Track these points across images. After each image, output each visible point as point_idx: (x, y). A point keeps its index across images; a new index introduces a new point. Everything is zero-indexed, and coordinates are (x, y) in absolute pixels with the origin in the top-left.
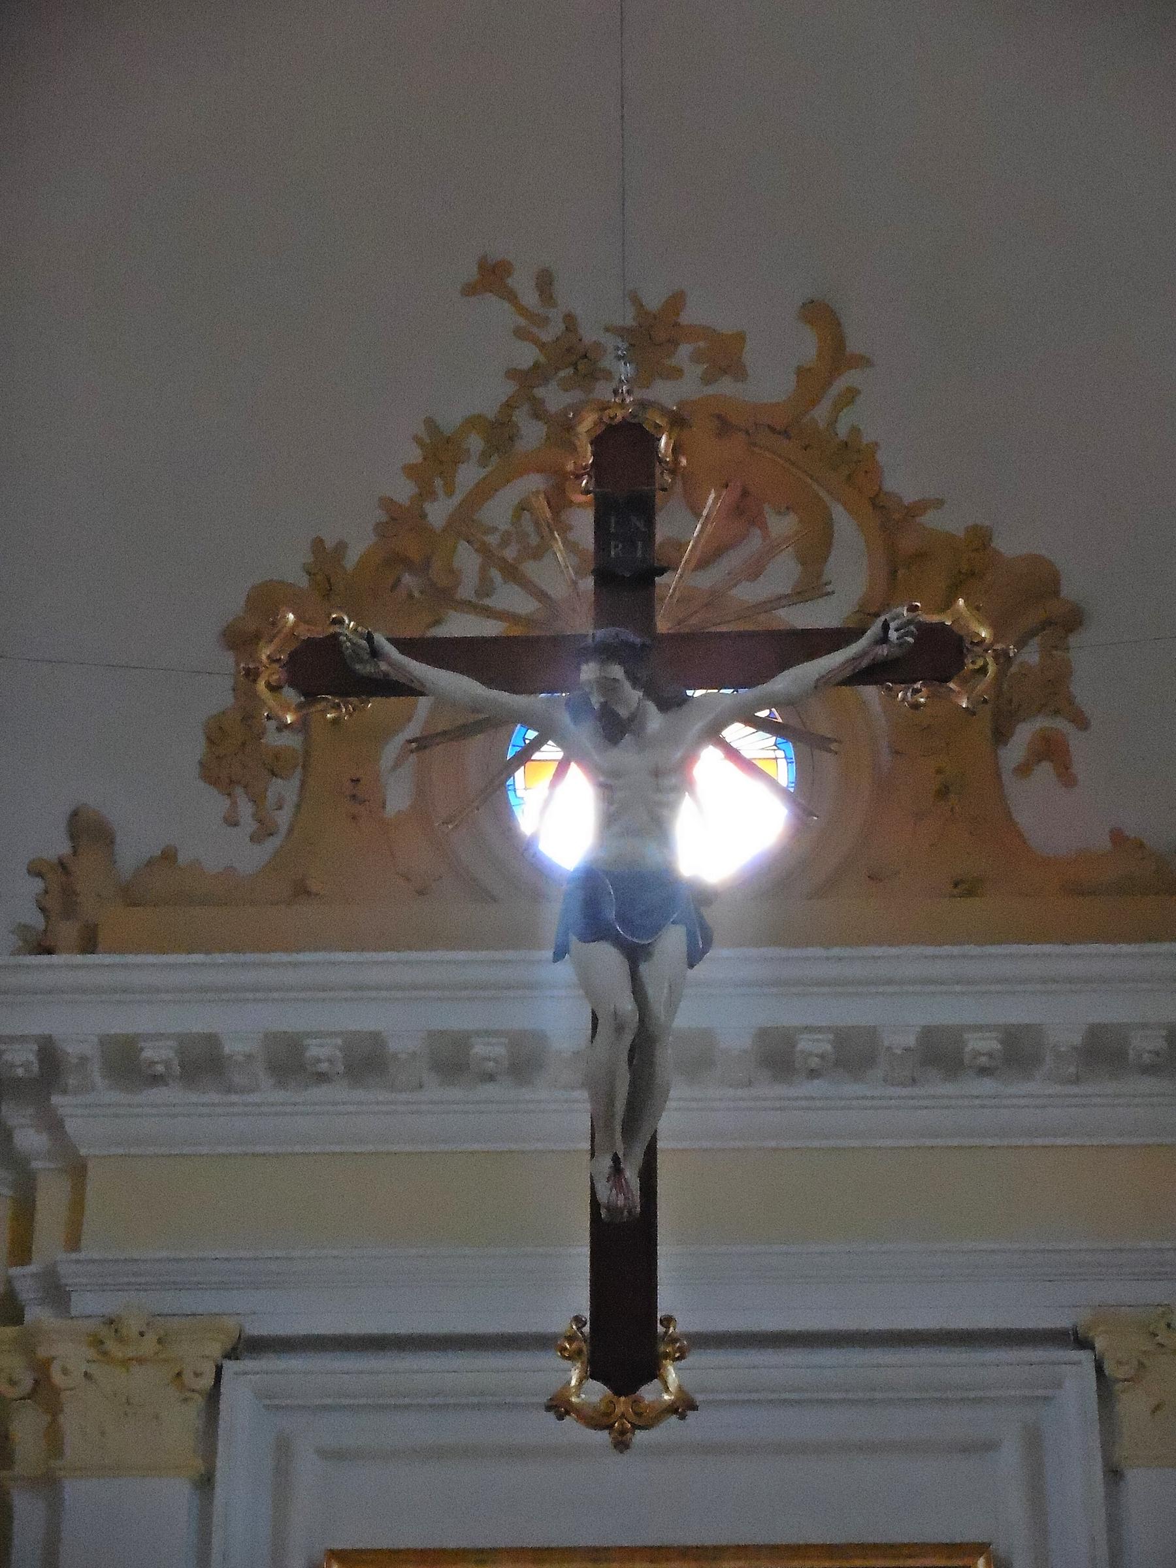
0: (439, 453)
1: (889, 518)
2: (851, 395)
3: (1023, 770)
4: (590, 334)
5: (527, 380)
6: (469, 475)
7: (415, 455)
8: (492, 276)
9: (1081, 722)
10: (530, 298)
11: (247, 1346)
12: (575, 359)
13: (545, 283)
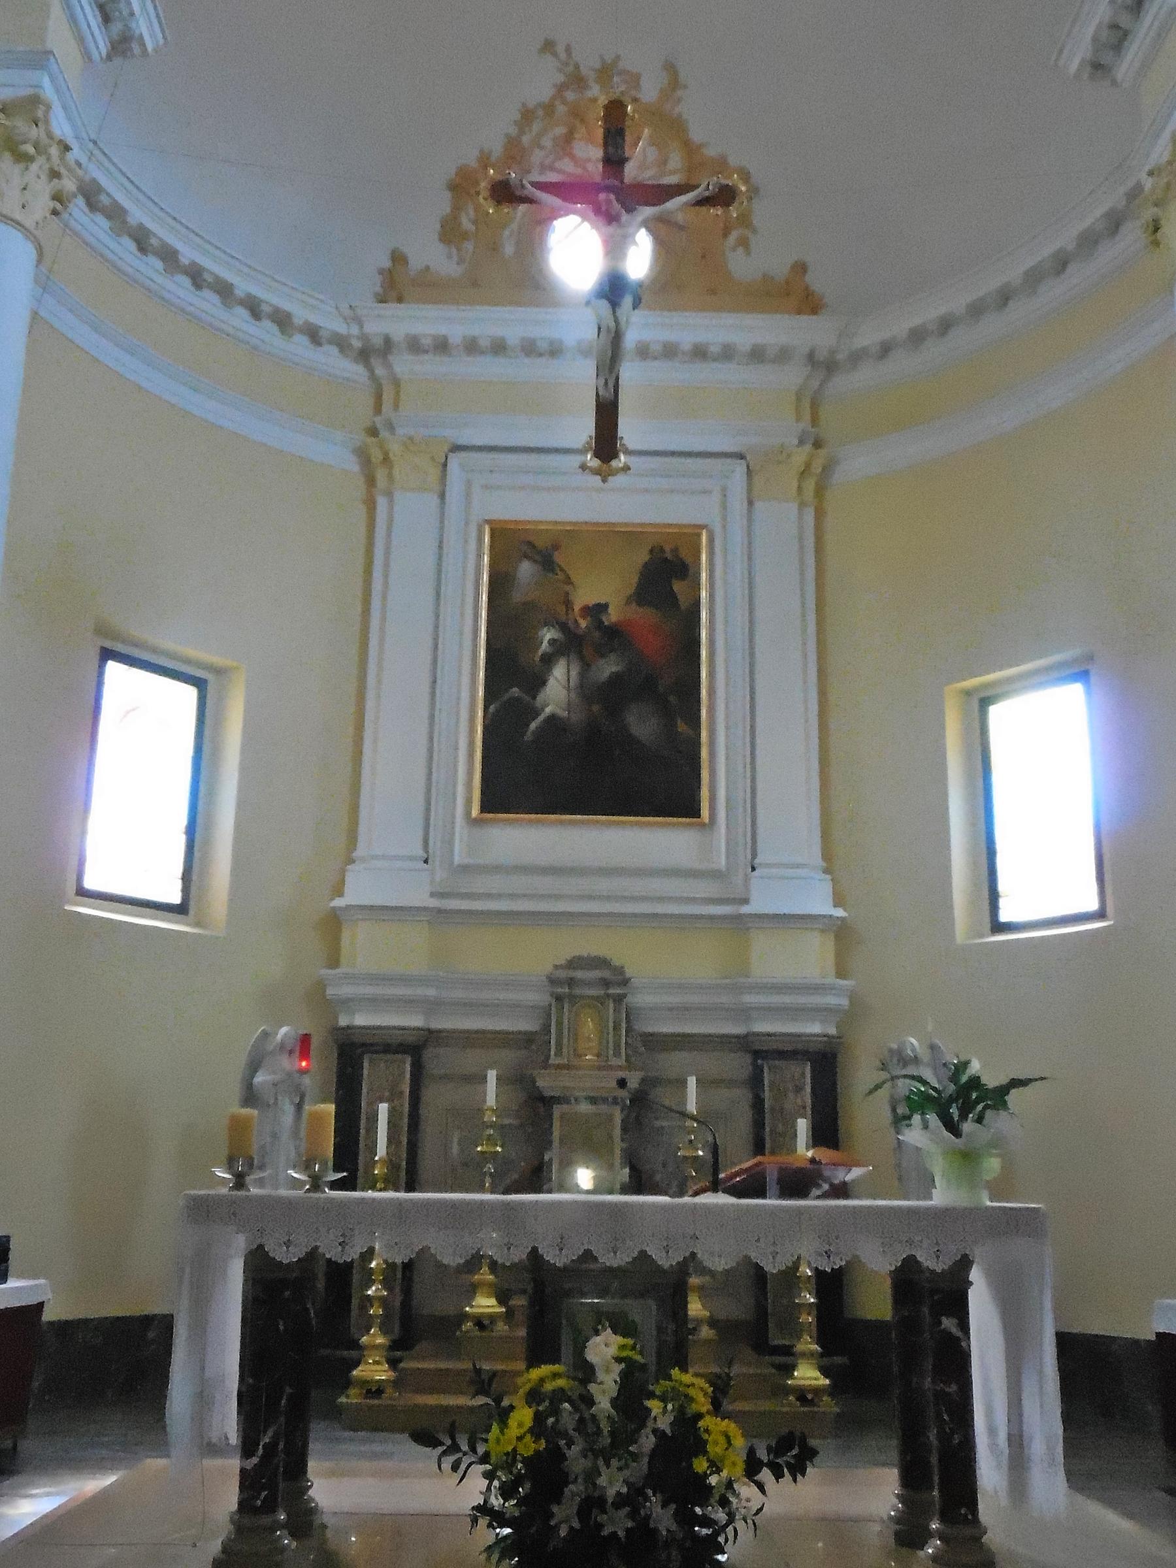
0: (527, 116)
1: (690, 149)
2: (679, 100)
3: (734, 249)
4: (584, 71)
5: (561, 88)
6: (536, 127)
7: (518, 116)
8: (548, 46)
9: (755, 231)
10: (563, 56)
11: (457, 448)
12: (577, 80)
13: (568, 49)
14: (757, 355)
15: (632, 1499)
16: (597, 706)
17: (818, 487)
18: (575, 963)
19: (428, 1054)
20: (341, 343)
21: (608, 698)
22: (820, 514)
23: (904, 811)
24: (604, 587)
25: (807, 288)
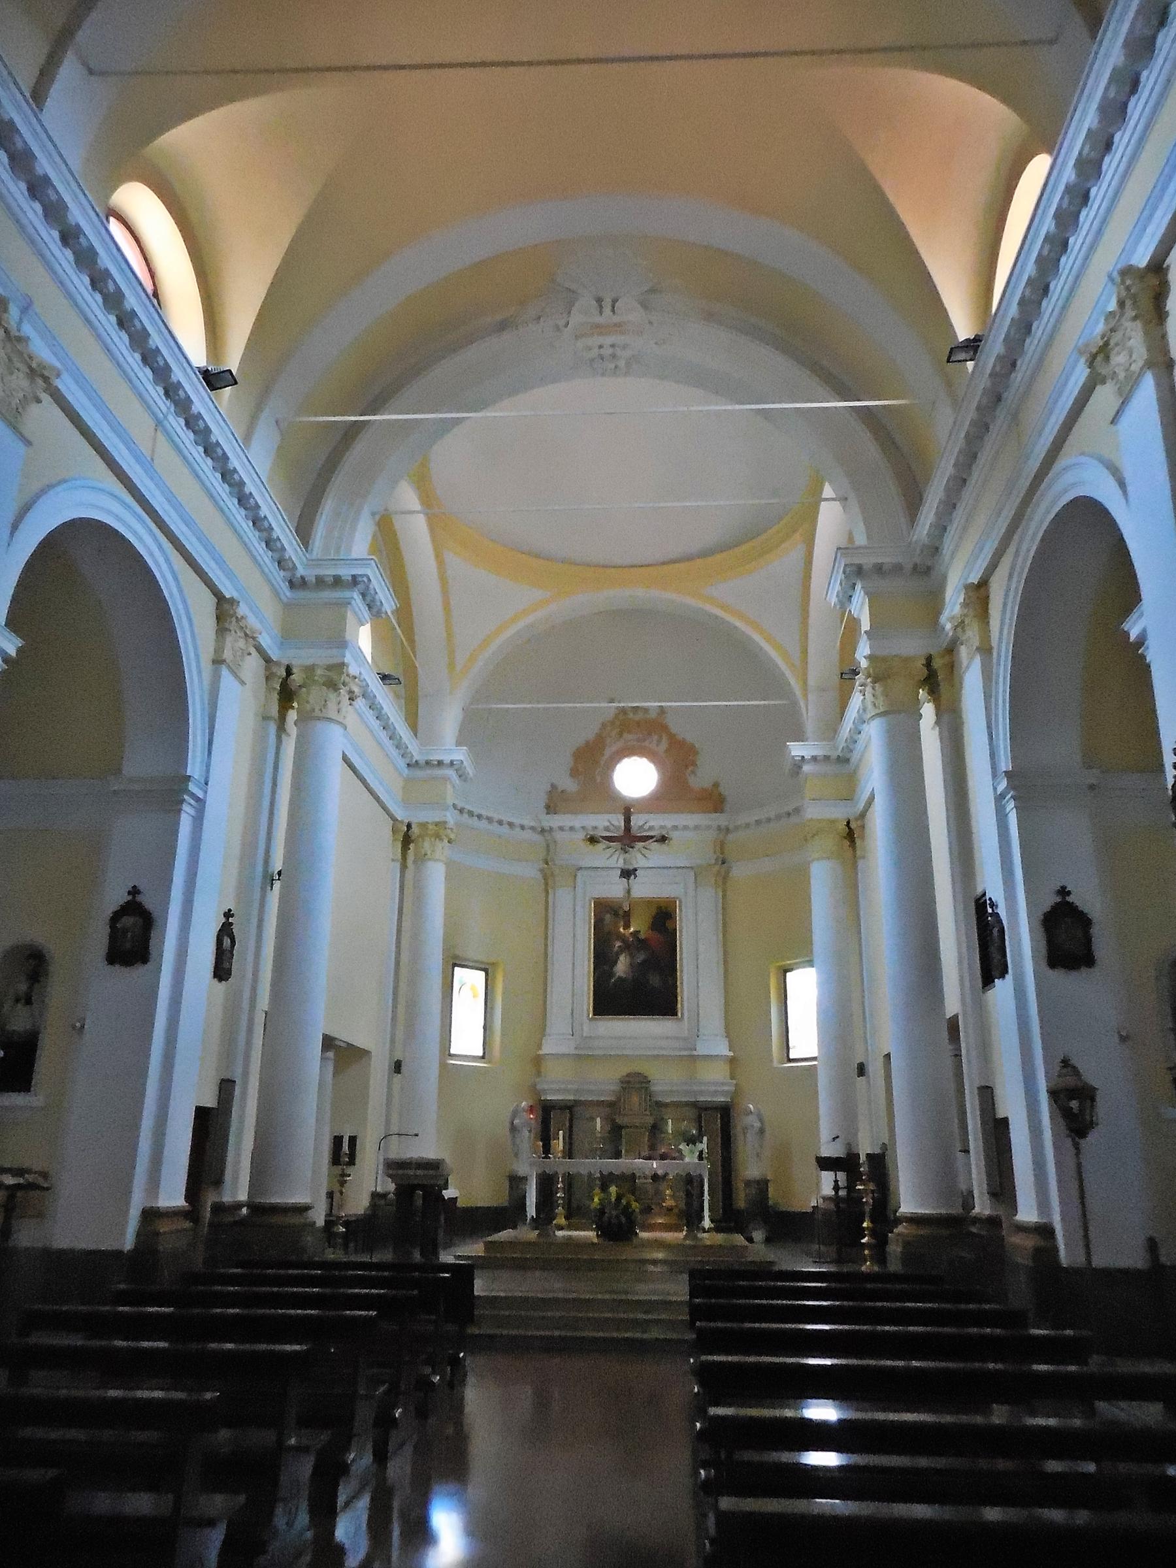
14: (696, 828)
15: (617, 1217)
16: (638, 973)
17: (724, 879)
18: (628, 1075)
19: (576, 1109)
20: (532, 828)
21: (641, 970)
22: (724, 891)
23: (754, 1012)
24: (638, 925)
25: (720, 794)
